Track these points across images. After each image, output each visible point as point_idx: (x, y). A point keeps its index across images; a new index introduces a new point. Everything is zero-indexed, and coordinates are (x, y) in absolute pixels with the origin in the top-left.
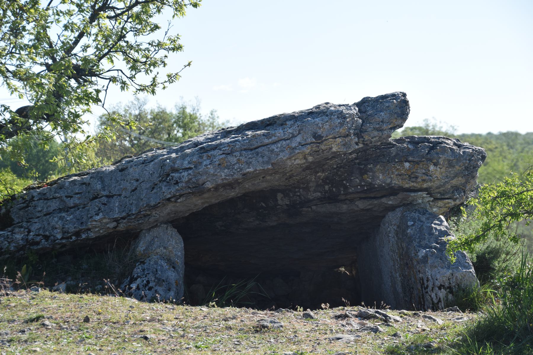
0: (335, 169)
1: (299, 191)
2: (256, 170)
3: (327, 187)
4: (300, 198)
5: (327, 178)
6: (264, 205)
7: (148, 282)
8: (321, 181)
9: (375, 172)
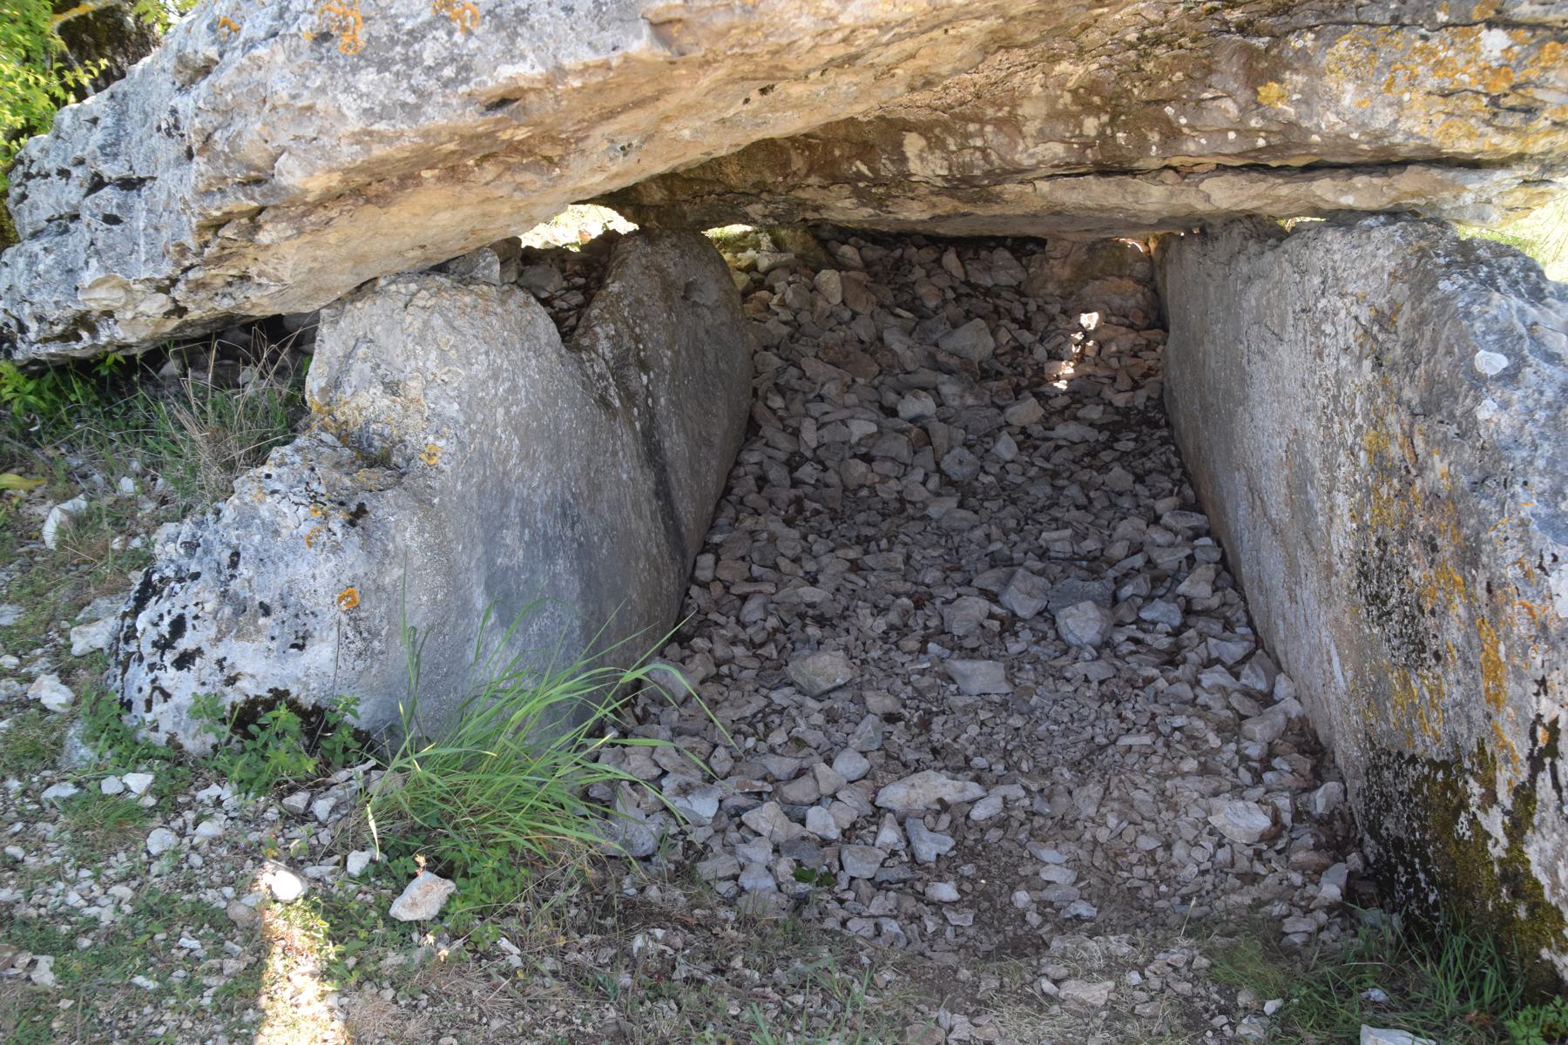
0: (1132, 46)
1: (981, 133)
2: (560, 72)
3: (1091, 125)
4: (986, 157)
5: (1093, 87)
6: (864, 169)
7: (178, 626)
8: (1068, 97)
9: (1321, 75)
